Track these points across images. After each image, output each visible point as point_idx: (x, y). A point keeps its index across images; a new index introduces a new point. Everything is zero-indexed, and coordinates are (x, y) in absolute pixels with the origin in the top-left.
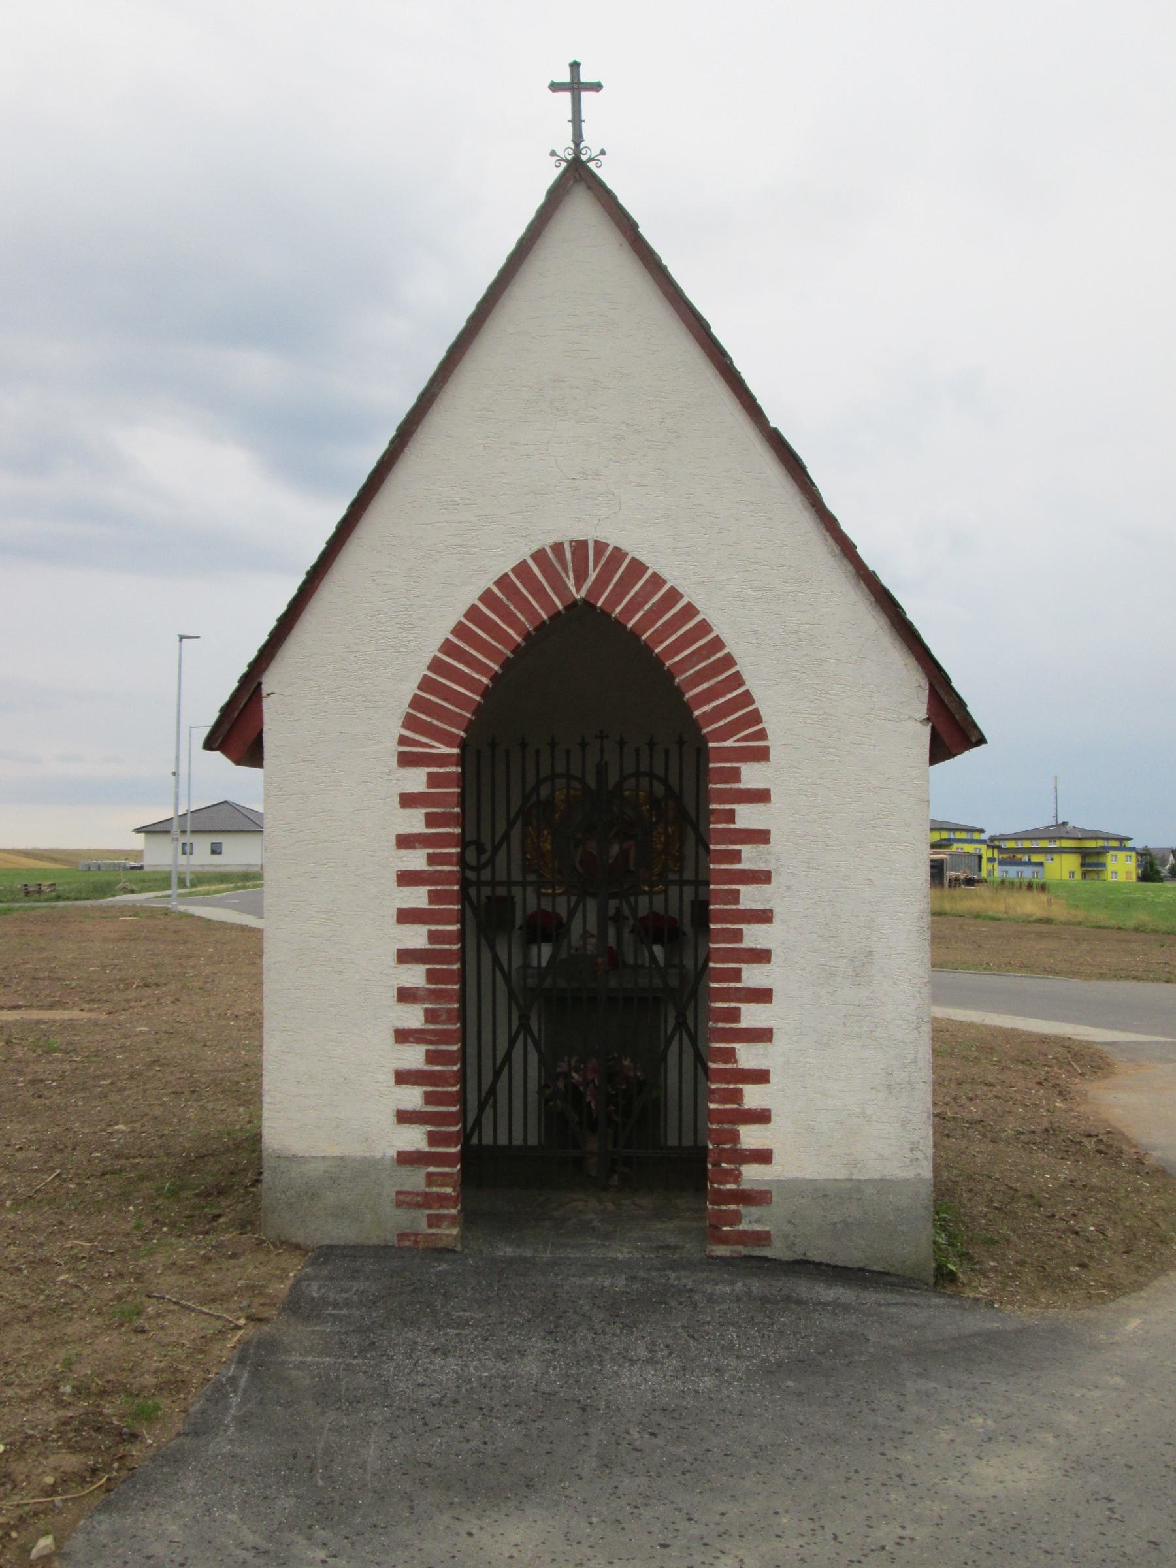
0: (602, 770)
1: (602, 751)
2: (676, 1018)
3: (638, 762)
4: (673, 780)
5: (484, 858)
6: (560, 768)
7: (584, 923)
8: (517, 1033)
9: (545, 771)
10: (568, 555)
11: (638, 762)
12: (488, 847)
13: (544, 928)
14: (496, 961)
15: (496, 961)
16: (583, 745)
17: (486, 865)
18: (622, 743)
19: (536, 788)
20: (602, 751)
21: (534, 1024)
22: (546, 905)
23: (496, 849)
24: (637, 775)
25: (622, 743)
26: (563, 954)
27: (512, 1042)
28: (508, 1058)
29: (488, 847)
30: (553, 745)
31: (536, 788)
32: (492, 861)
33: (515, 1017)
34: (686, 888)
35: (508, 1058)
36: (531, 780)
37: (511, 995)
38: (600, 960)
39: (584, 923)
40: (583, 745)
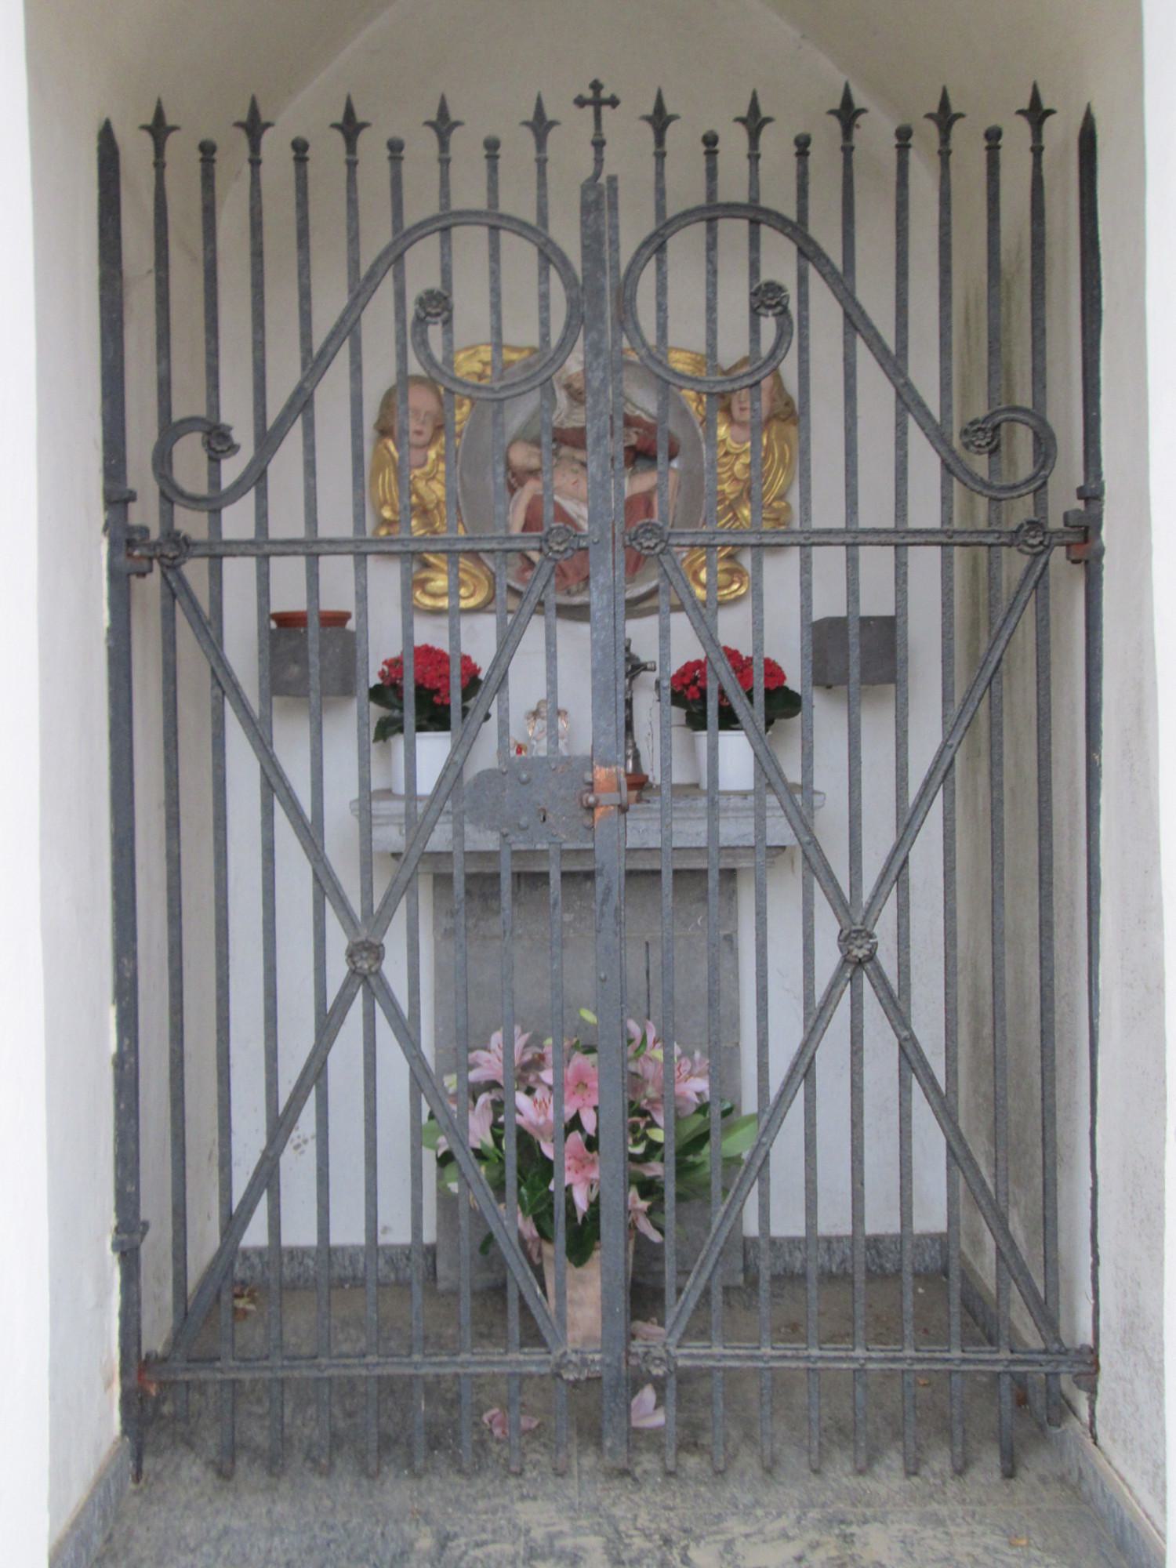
0: (599, 199)
1: (599, 144)
2: (845, 940)
3: (712, 173)
4: (826, 233)
5: (231, 470)
6: (469, 194)
7: (548, 683)
8: (344, 1001)
9: (421, 206)
10: (609, 311)
11: (712, 173)
12: (243, 434)
13: (430, 695)
14: (273, 783)
15: (273, 783)
16: (541, 125)
17: (238, 490)
18: (660, 120)
19: (394, 257)
20: (599, 144)
21: (394, 970)
22: (430, 634)
23: (268, 441)
24: (711, 213)
25: (660, 120)
26: (485, 756)
27: (327, 1024)
28: (315, 1073)
29: (243, 434)
30: (443, 125)
31: (394, 257)
32: (256, 478)
33: (338, 941)
34: (724, 225)
35: (315, 1073)
36: (377, 238)
37: (325, 885)
38: (601, 774)
39: (548, 683)
40: (541, 125)
